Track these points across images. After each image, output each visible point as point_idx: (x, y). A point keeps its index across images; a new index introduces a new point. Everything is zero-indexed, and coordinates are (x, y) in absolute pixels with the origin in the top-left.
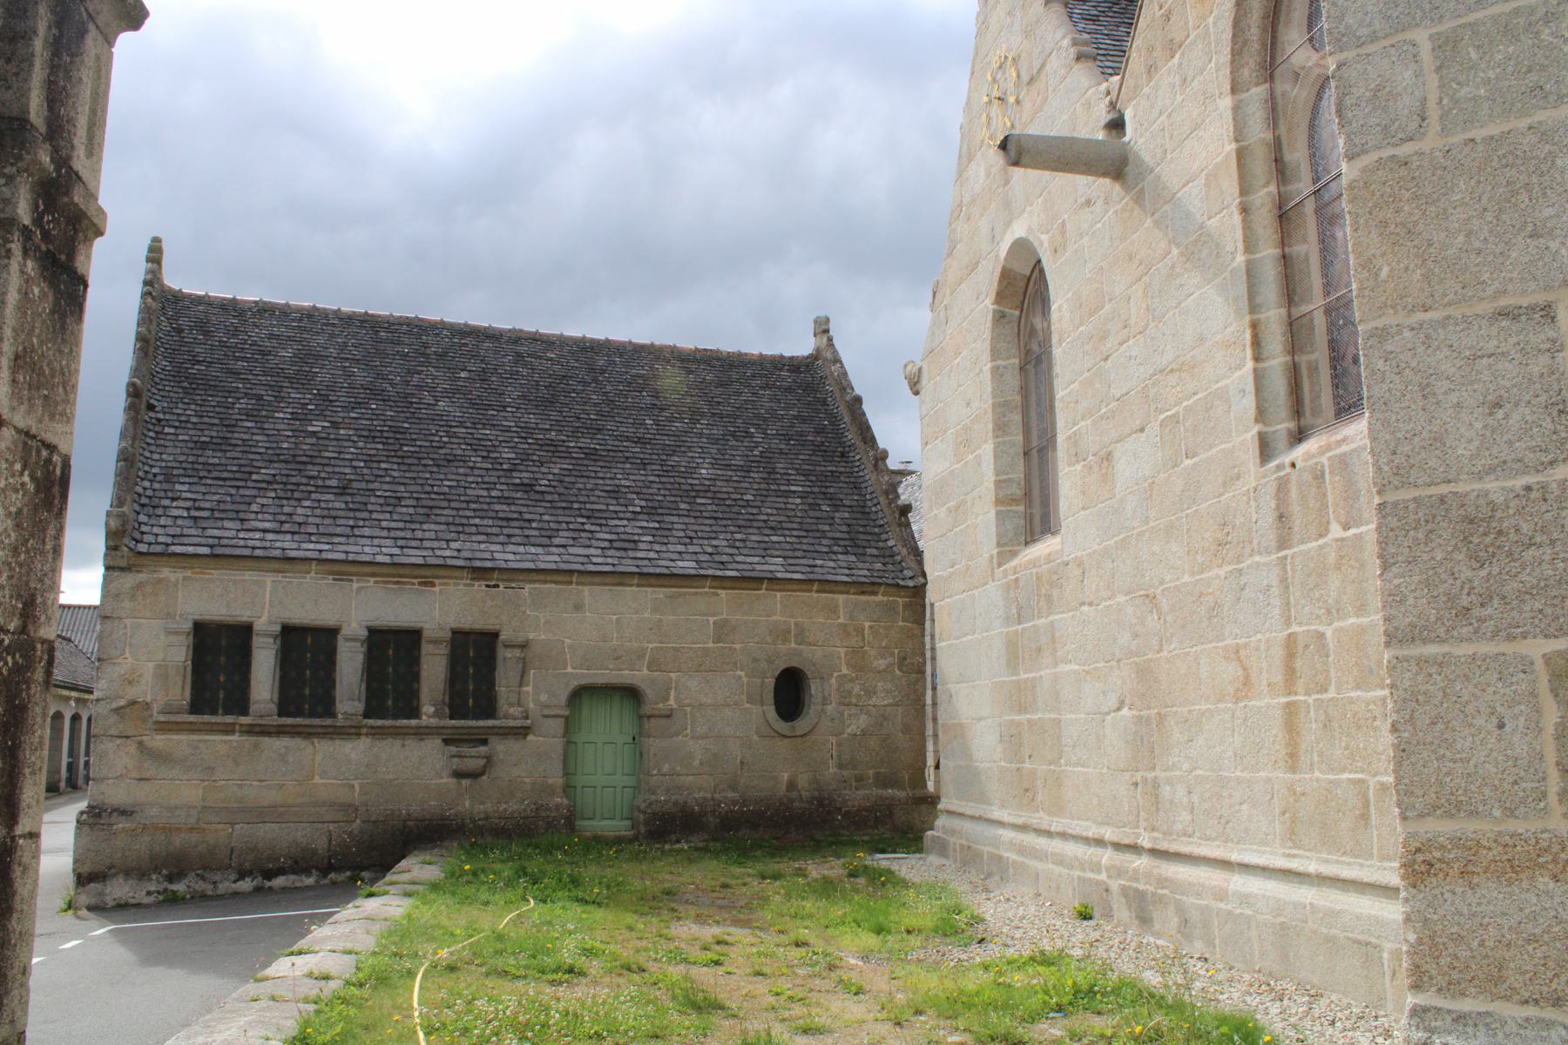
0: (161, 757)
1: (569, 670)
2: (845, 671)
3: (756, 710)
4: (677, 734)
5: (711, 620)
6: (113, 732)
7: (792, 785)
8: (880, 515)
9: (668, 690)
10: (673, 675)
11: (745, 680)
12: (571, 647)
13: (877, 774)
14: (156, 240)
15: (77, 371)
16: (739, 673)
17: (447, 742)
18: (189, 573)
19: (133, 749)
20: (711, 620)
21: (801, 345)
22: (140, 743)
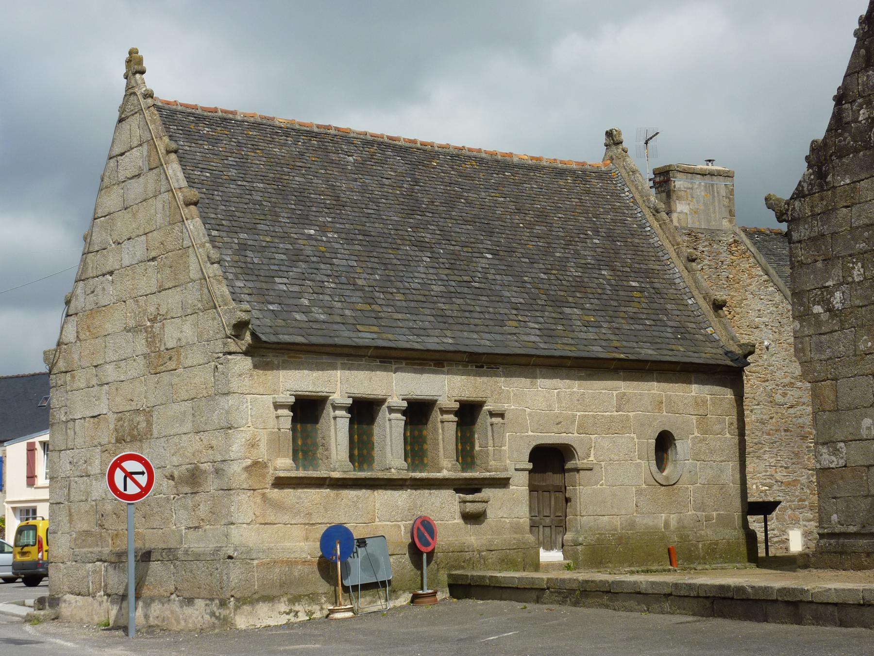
0: (278, 506)
1: (530, 433)
2: (696, 434)
3: (643, 463)
4: (596, 483)
5: (615, 393)
6: (245, 486)
7: (667, 524)
8: (672, 265)
9: (589, 449)
10: (593, 437)
11: (636, 440)
12: (530, 414)
13: (719, 515)
14: (132, 52)
15: (492, 154)
16: (632, 435)
17: (457, 491)
18: (286, 358)
19: (258, 500)
20: (615, 393)
21: (593, 154)
22: (264, 495)
